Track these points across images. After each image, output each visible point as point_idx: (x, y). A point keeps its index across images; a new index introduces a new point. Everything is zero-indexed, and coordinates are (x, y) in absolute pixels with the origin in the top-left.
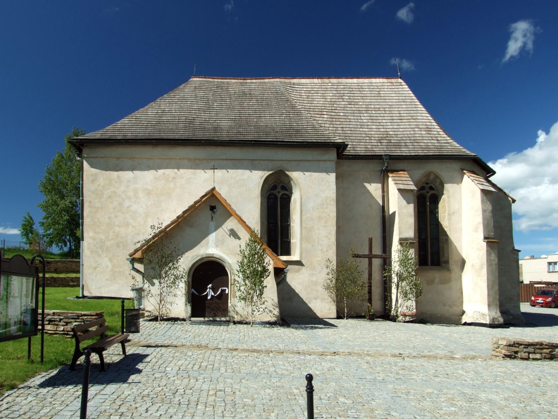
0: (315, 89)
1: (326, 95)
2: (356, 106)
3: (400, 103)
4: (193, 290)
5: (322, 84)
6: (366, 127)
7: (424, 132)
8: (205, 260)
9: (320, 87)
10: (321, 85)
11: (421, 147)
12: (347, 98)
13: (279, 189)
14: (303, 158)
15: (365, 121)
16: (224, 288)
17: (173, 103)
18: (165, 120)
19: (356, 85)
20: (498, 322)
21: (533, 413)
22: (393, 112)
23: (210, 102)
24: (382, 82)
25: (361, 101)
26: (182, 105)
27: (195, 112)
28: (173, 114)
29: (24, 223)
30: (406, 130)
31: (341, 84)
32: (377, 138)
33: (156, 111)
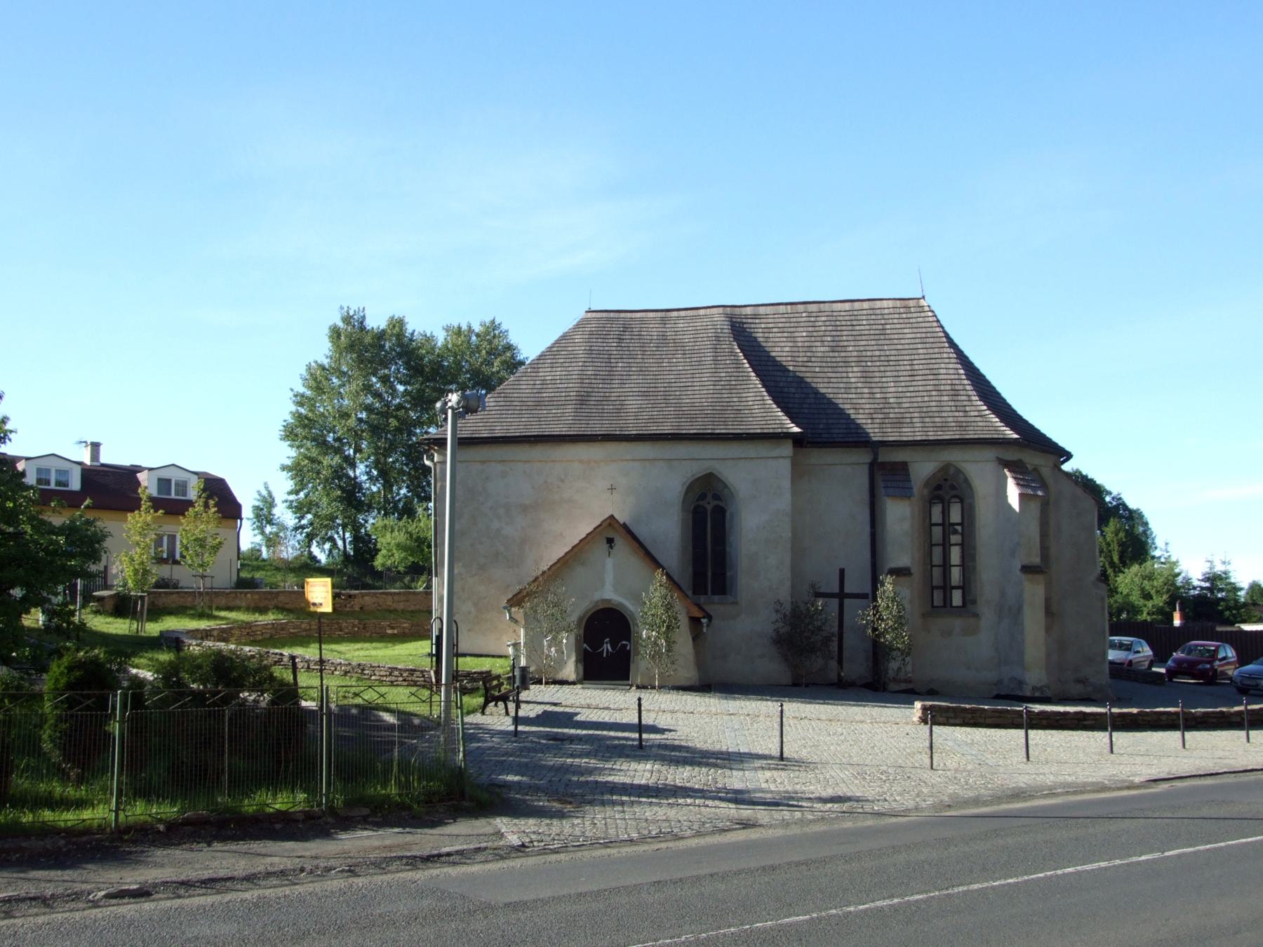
0: (780, 325)
1: (796, 334)
2: (843, 354)
3: (915, 346)
4: (585, 645)
5: (792, 315)
6: (853, 391)
7: (946, 398)
8: (601, 607)
9: (788, 320)
10: (790, 315)
11: (934, 425)
12: (829, 339)
13: (709, 496)
14: (743, 456)
15: (853, 380)
16: (624, 642)
17: (557, 365)
18: (547, 399)
19: (848, 313)
20: (1042, 693)
21: (253, 566)
22: (901, 363)
23: (612, 361)
24: (891, 306)
25: (852, 343)
26: (570, 369)
27: (590, 381)
28: (558, 386)
29: (257, 503)
30: (917, 394)
31: (823, 314)
32: (867, 411)
33: (532, 382)
